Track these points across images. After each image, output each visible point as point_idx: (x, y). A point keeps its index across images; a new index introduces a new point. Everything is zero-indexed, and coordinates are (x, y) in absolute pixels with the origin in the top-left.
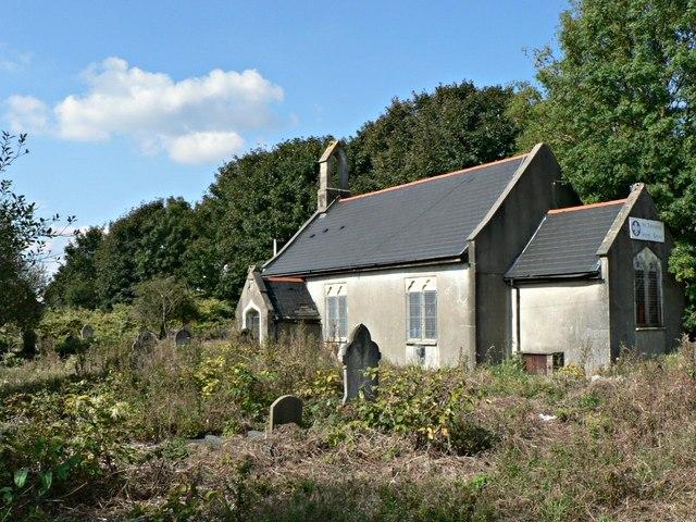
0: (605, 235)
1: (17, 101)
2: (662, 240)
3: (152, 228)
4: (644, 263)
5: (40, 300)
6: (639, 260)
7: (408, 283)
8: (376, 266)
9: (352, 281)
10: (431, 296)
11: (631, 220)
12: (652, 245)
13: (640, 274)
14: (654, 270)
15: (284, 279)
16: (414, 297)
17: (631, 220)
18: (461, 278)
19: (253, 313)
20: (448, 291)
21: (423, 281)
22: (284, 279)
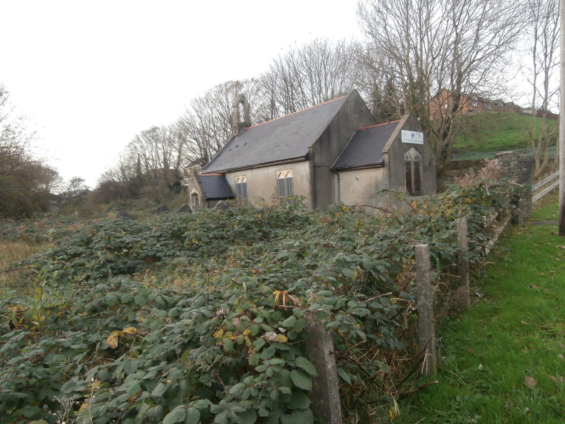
0: (387, 141)
1: (143, 173)
2: (422, 143)
3: (140, 241)
4: (411, 157)
5: (23, 180)
6: (408, 155)
7: (278, 173)
8: (260, 164)
9: (249, 173)
10: (289, 180)
11: (403, 131)
12: (416, 146)
13: (408, 163)
14: (417, 160)
15: (207, 175)
16: (280, 181)
17: (403, 131)
18: (305, 168)
19: (195, 194)
20: (299, 178)
21: (285, 173)
22: (207, 175)
